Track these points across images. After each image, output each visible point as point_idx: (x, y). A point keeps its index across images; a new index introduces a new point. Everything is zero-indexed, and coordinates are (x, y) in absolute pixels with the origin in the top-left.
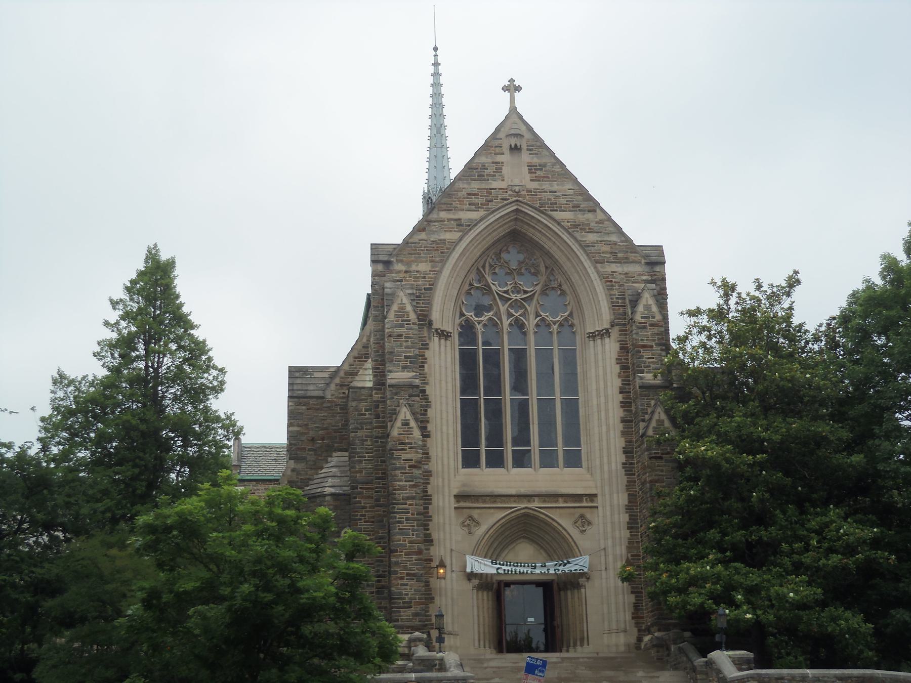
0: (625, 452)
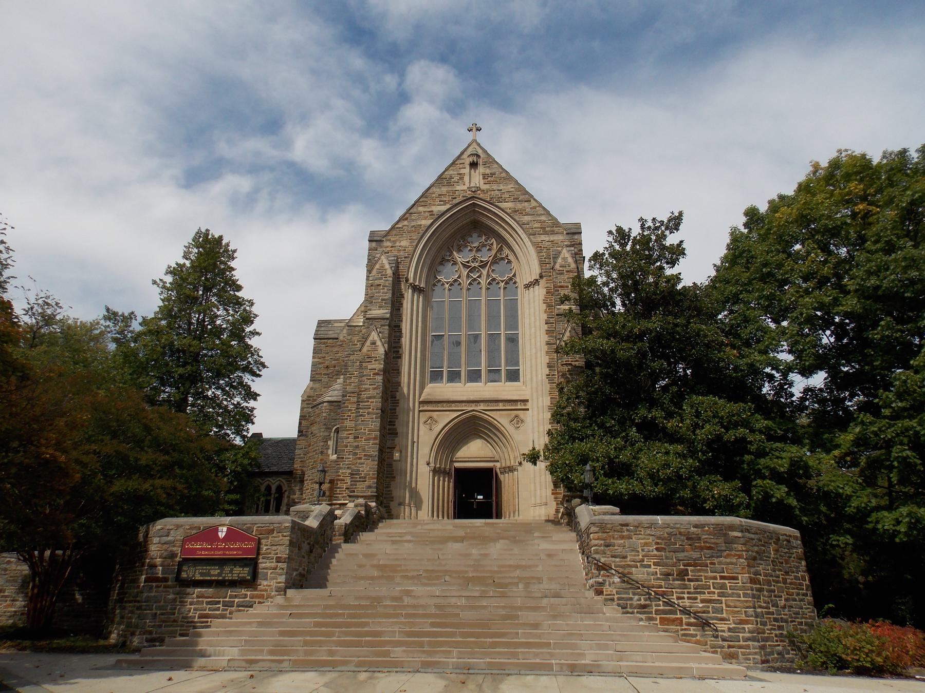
0: (549, 367)
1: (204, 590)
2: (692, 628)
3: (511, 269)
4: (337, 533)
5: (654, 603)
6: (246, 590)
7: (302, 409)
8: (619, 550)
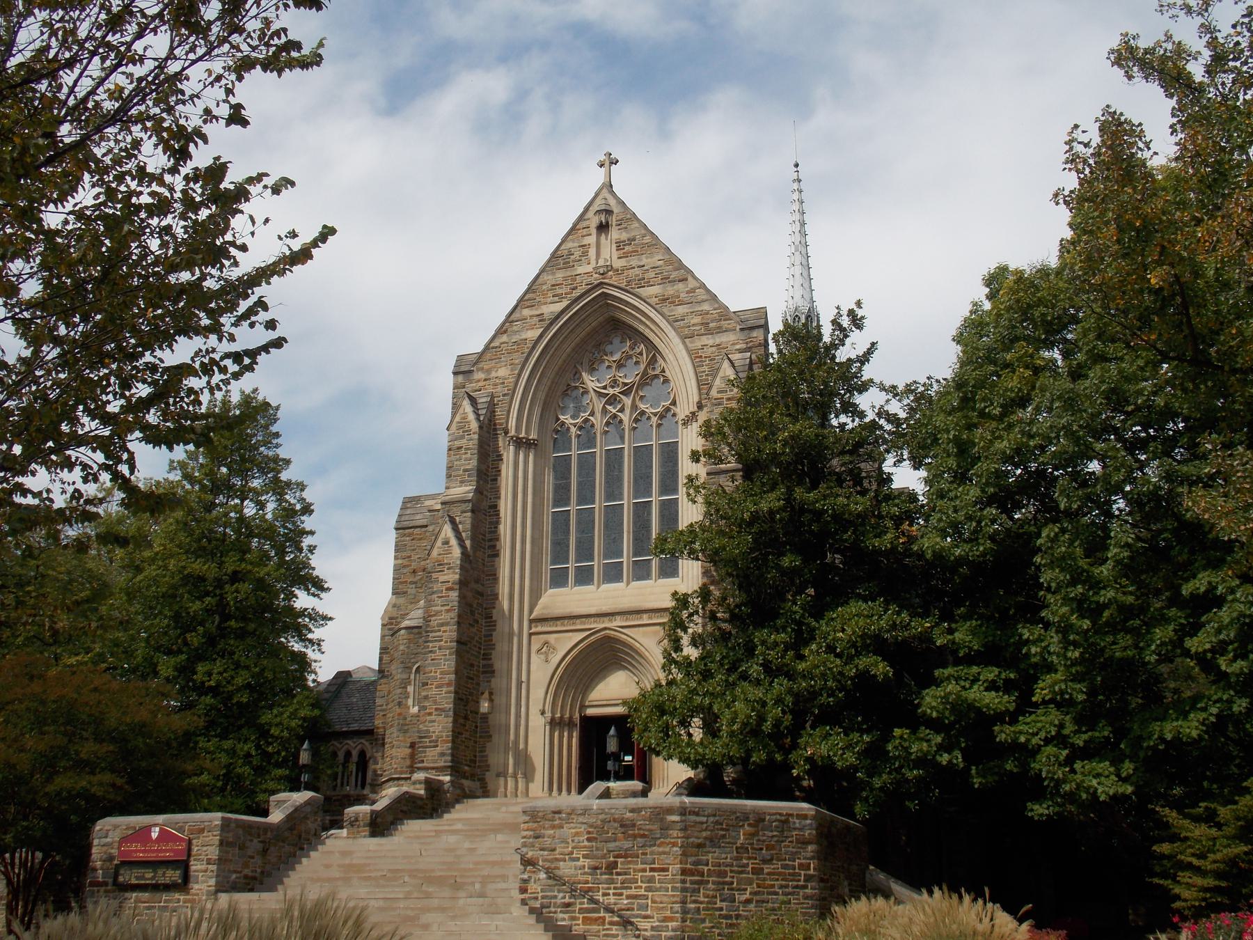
2: (614, 927)
4: (362, 823)
5: (578, 901)
7: (383, 637)
8: (548, 842)
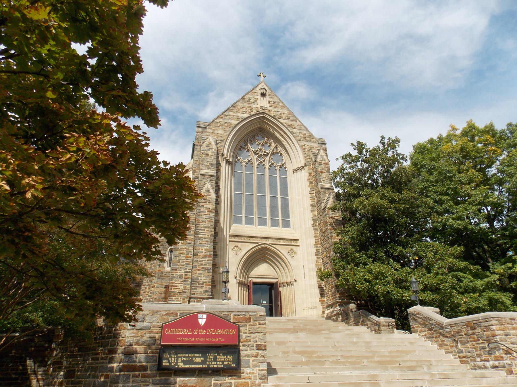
1: (186, 379)
3: (282, 160)
6: (230, 378)
